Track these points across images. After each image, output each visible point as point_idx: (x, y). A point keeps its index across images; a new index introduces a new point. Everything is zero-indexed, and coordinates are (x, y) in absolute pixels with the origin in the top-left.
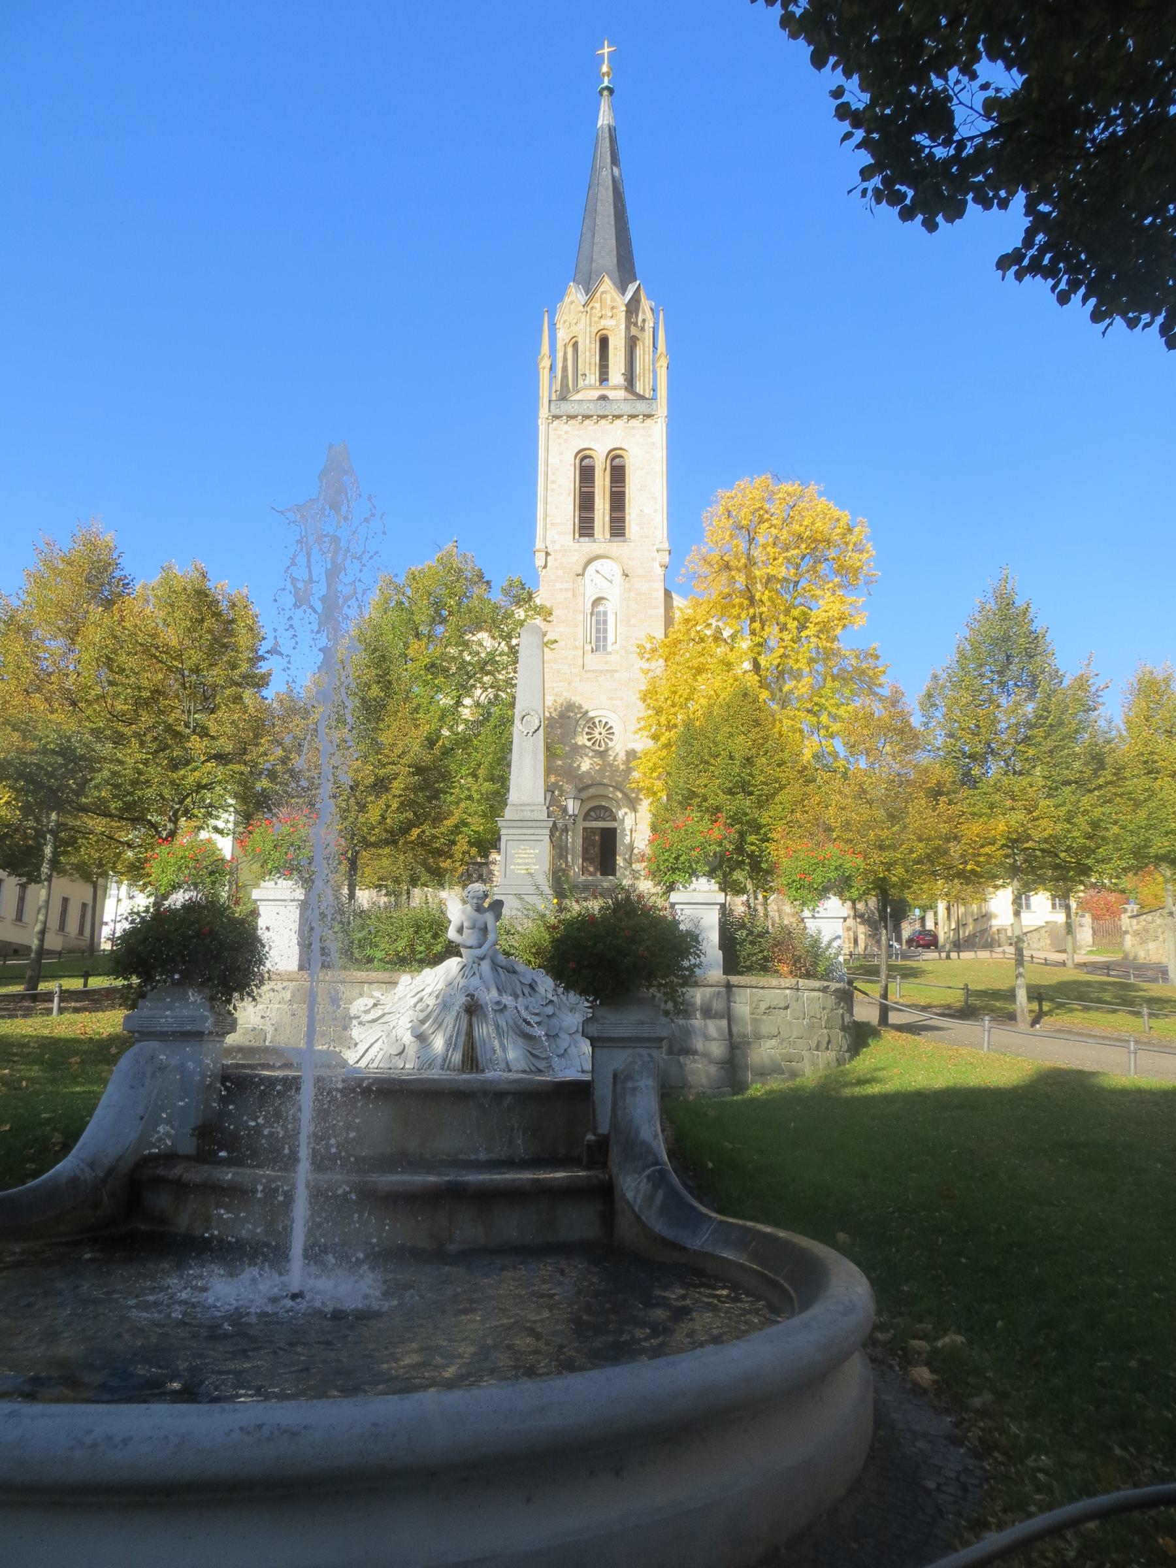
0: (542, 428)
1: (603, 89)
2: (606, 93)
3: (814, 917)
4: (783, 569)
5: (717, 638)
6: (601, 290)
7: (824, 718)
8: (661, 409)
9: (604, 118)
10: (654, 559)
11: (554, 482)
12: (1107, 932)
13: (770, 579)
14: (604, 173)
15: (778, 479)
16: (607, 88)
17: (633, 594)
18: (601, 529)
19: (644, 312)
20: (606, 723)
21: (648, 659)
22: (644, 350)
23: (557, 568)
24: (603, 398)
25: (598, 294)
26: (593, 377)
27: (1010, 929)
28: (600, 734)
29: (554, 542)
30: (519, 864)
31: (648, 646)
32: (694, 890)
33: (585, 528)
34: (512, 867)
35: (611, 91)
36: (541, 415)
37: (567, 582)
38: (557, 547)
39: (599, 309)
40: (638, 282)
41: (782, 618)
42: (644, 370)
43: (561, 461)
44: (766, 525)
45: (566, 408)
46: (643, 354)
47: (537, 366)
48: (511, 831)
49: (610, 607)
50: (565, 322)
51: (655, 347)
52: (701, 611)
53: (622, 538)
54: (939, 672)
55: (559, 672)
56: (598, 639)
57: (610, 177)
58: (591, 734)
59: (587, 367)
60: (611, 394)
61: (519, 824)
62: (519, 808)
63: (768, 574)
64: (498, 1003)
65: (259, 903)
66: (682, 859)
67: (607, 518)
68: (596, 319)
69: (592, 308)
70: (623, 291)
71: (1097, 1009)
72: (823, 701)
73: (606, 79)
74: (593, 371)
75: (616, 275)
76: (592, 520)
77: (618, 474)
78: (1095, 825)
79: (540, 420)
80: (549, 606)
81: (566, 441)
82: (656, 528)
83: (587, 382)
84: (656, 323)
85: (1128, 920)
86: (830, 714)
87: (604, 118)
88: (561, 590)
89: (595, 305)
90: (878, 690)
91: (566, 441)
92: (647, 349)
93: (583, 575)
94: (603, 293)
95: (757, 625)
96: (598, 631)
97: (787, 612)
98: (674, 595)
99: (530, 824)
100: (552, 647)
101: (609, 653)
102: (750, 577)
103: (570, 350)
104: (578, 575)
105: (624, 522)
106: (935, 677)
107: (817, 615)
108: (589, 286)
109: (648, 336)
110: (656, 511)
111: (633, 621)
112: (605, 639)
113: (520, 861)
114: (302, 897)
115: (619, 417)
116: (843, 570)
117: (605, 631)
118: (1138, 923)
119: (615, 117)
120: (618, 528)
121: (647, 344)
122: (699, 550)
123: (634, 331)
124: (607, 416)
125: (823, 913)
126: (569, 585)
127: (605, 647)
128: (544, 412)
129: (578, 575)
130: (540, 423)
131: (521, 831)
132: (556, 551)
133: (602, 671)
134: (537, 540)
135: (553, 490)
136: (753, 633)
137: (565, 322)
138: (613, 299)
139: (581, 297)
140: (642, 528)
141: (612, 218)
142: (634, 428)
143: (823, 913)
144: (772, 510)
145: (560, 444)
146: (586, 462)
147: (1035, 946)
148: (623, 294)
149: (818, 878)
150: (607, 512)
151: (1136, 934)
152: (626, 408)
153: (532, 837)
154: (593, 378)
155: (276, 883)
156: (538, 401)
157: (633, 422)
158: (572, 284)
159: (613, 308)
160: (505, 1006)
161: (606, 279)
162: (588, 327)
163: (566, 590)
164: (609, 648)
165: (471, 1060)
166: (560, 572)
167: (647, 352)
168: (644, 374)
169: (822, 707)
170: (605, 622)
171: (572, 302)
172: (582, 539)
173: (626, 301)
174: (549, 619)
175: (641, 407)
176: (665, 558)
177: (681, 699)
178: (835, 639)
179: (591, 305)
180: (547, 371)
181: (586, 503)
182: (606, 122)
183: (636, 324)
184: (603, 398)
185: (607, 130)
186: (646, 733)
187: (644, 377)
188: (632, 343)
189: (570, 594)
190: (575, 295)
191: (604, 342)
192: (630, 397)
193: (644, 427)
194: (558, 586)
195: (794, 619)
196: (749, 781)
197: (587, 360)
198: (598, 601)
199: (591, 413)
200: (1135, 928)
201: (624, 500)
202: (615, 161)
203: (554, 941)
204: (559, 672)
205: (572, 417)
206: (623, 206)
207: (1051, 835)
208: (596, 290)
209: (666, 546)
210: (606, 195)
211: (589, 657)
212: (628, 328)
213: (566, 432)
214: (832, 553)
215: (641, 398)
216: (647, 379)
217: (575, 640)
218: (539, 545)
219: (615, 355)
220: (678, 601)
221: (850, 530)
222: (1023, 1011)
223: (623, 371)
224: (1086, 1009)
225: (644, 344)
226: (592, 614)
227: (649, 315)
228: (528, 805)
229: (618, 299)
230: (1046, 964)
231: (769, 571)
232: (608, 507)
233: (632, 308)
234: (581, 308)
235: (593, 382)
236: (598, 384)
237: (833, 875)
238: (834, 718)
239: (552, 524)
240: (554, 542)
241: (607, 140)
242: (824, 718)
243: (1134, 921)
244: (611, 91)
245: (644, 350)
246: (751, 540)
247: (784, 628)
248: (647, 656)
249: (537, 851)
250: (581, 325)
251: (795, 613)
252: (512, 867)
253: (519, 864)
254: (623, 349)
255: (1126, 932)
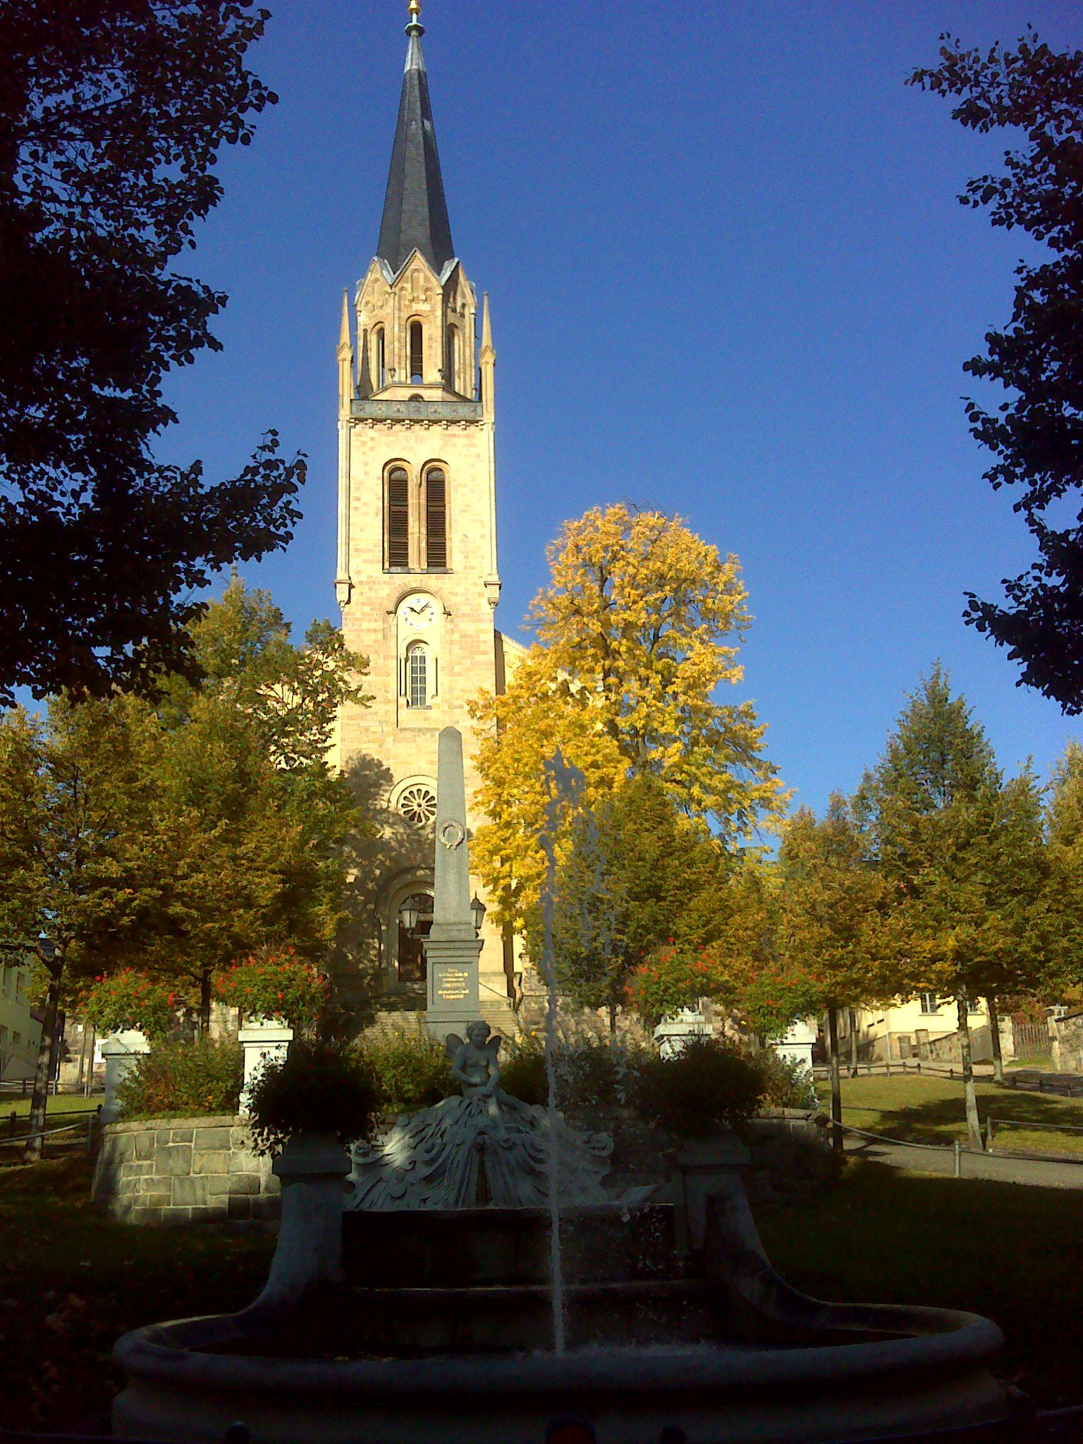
0: (343, 434)
1: (410, 29)
2: (414, 33)
3: (782, 1044)
4: (644, 615)
5: (565, 690)
6: (412, 267)
7: (696, 790)
8: (489, 417)
9: (412, 62)
10: (481, 595)
11: (358, 499)
12: (1033, 1039)
13: (629, 625)
14: (413, 127)
15: (634, 508)
16: (416, 27)
17: (456, 637)
18: (416, 555)
19: (464, 296)
20: (427, 792)
21: (481, 718)
22: (464, 341)
23: (363, 604)
24: (416, 398)
25: (408, 273)
26: (403, 372)
27: (913, 1036)
28: (420, 806)
29: (359, 572)
30: (447, 989)
31: (481, 703)
32: (682, 1021)
33: (397, 556)
34: (440, 992)
35: (420, 31)
36: (341, 418)
37: (376, 621)
38: (363, 578)
39: (410, 289)
40: (456, 260)
41: (642, 671)
42: (464, 364)
43: (366, 473)
44: (622, 563)
45: (371, 409)
46: (463, 347)
47: (336, 356)
48: (437, 953)
49: (429, 652)
50: (367, 303)
51: (478, 337)
52: (548, 662)
53: (441, 569)
54: (872, 772)
55: (367, 730)
56: (414, 691)
57: (420, 132)
58: (407, 806)
59: (397, 360)
60: (427, 394)
61: (447, 945)
62: (445, 927)
63: (625, 620)
64: (507, 1140)
65: (245, 1045)
66: (671, 991)
67: (424, 545)
68: (407, 303)
69: (402, 289)
70: (438, 270)
71: (1025, 1128)
72: (693, 769)
73: (414, 16)
74: (403, 365)
75: (430, 249)
76: (405, 546)
77: (436, 489)
78: (1043, 937)
79: (340, 423)
80: (365, 656)
81: (372, 449)
82: (483, 557)
83: (396, 379)
84: (479, 308)
85: (1055, 1024)
86: (702, 786)
87: (412, 62)
88: (369, 630)
89: (405, 285)
90: (756, 754)
91: (372, 449)
92: (468, 341)
93: (395, 613)
94: (416, 270)
95: (612, 680)
96: (414, 680)
97: (649, 666)
98: (504, 637)
99: (458, 945)
100: (368, 704)
101: (429, 708)
102: (606, 624)
103: (373, 339)
104: (389, 613)
105: (445, 550)
106: (868, 778)
107: (685, 669)
108: (396, 260)
109: (469, 321)
110: (483, 537)
111: (457, 669)
112: (424, 690)
113: (449, 985)
114: (291, 1038)
115: (436, 422)
116: (709, 615)
117: (424, 680)
118: (1066, 1028)
119: (426, 63)
120: (437, 558)
121: (467, 335)
122: (545, 593)
123: (452, 318)
124: (422, 421)
125: (791, 1040)
126: (379, 625)
127: (423, 701)
128: (345, 413)
129: (389, 613)
130: (339, 427)
131: (460, 953)
132: (361, 583)
133: (420, 730)
134: (339, 569)
135: (356, 509)
136: (608, 688)
137: (367, 303)
138: (427, 279)
139: (389, 276)
140: (466, 557)
141: (424, 180)
142: (454, 436)
143: (791, 1040)
144: (630, 545)
145: (364, 453)
146: (397, 475)
147: (946, 1057)
148: (439, 274)
149: (785, 1005)
150: (424, 536)
151: (1064, 1040)
152: (445, 412)
153: (461, 960)
154: (403, 374)
155: (262, 1024)
156: (338, 400)
157: (454, 429)
158: (376, 258)
159: (427, 290)
160: (514, 1143)
161: (418, 254)
162: (397, 312)
163: (375, 631)
164: (428, 703)
165: (484, 1194)
166: (367, 609)
167: (468, 344)
168: (465, 369)
169: (694, 779)
170: (423, 670)
171: (376, 280)
172: (393, 569)
173: (443, 282)
174: (365, 671)
175: (464, 411)
176: (494, 593)
177: (527, 769)
178: (705, 697)
179: (400, 285)
180: (347, 364)
181: (396, 524)
182: (415, 67)
183: (454, 310)
184: (416, 398)
185: (416, 76)
186: (483, 809)
187: (465, 373)
188: (449, 332)
189: (380, 636)
190: (379, 274)
191: (416, 331)
192: (449, 397)
193: (467, 436)
194: (365, 625)
195: (657, 672)
196: (662, 885)
197: (396, 351)
198: (413, 644)
199: (401, 416)
200: (1064, 1033)
201: (444, 523)
202: (426, 113)
203: (358, 1071)
204: (367, 730)
205: (377, 421)
206: (438, 168)
207: (1000, 948)
208: (405, 268)
209: (495, 579)
210: (415, 153)
211: (404, 712)
212: (444, 315)
213: (373, 439)
214: (697, 594)
215: (464, 399)
216: (468, 377)
217: (386, 692)
218: (341, 575)
219: (430, 347)
220: (512, 649)
221: (718, 568)
222: (974, 1134)
223: (440, 367)
224: (1015, 1128)
225: (464, 334)
226: (406, 660)
227: (470, 300)
228: (455, 924)
229: (433, 280)
230: (952, 1078)
231: (625, 616)
232: (424, 530)
233: (450, 288)
234: (388, 289)
235: (403, 379)
236: (409, 381)
237: (801, 1000)
238: (706, 789)
239: (357, 550)
240: (359, 572)
241: (417, 88)
242: (696, 790)
243: (1062, 1025)
244: (420, 31)
245: (464, 341)
246: (604, 580)
247: (644, 681)
248: (479, 714)
249: (466, 974)
250: (389, 309)
251: (659, 665)
252: (440, 992)
253: (447, 989)
254: (440, 340)
255: (1054, 1039)
